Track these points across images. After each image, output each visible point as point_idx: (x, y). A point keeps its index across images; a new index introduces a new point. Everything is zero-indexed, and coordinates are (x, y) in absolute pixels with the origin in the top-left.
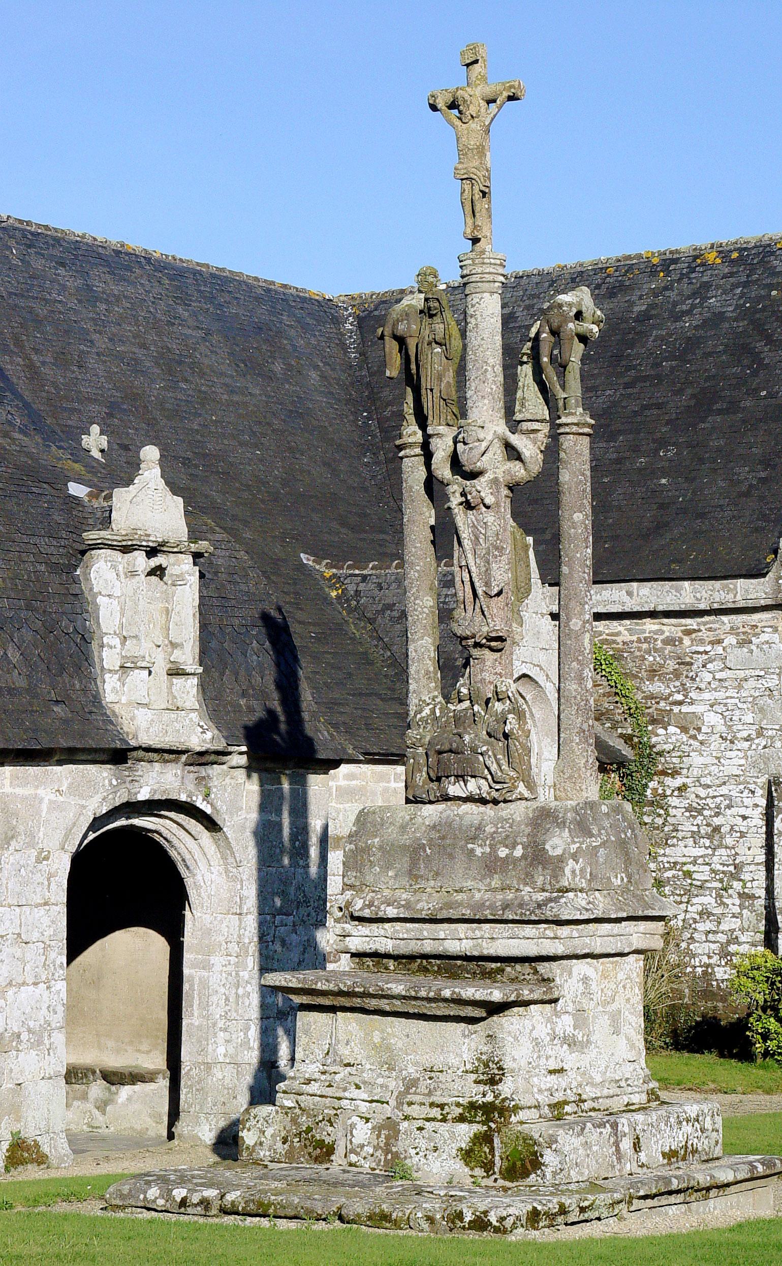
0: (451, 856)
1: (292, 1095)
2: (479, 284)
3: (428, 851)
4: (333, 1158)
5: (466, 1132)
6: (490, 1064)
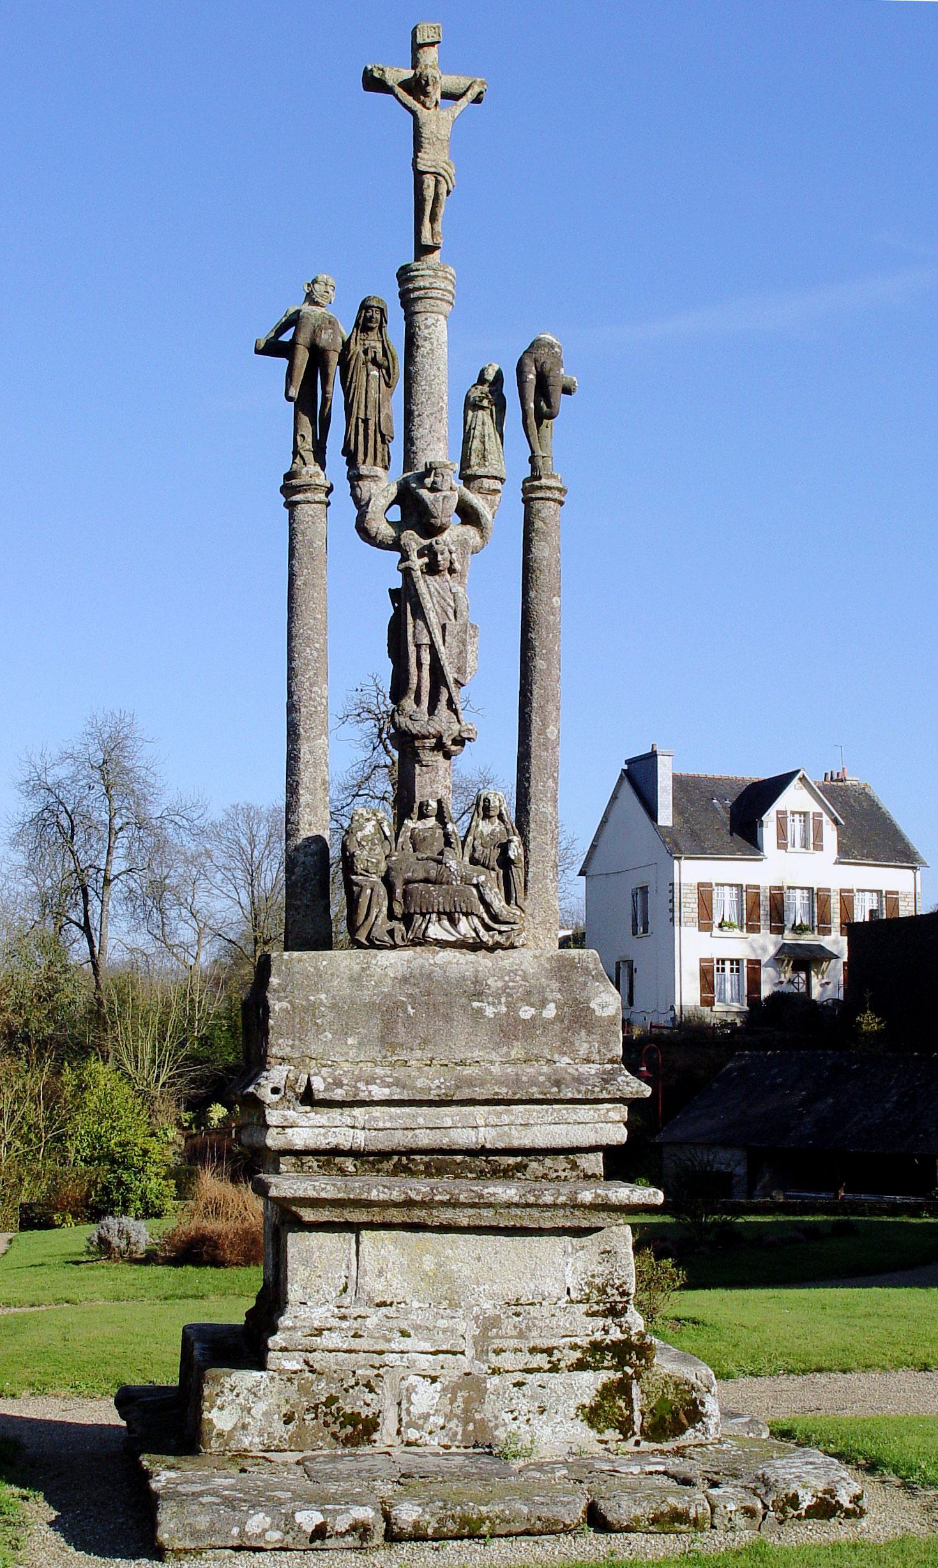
0: (447, 1018)
1: (296, 1353)
2: (439, 302)
3: (411, 1011)
4: (375, 1436)
5: (589, 1384)
6: (608, 1289)
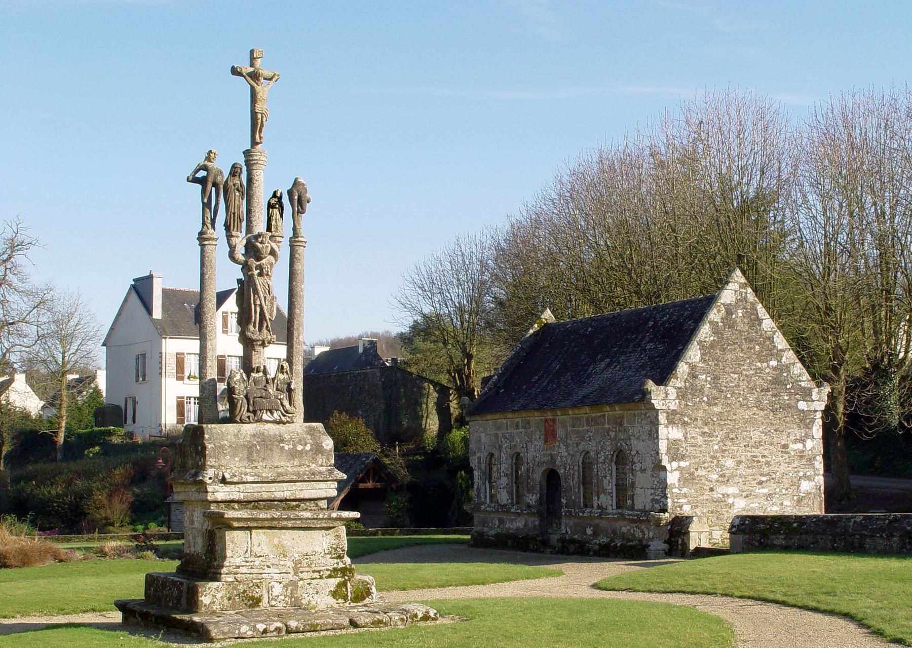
5: (334, 582)
